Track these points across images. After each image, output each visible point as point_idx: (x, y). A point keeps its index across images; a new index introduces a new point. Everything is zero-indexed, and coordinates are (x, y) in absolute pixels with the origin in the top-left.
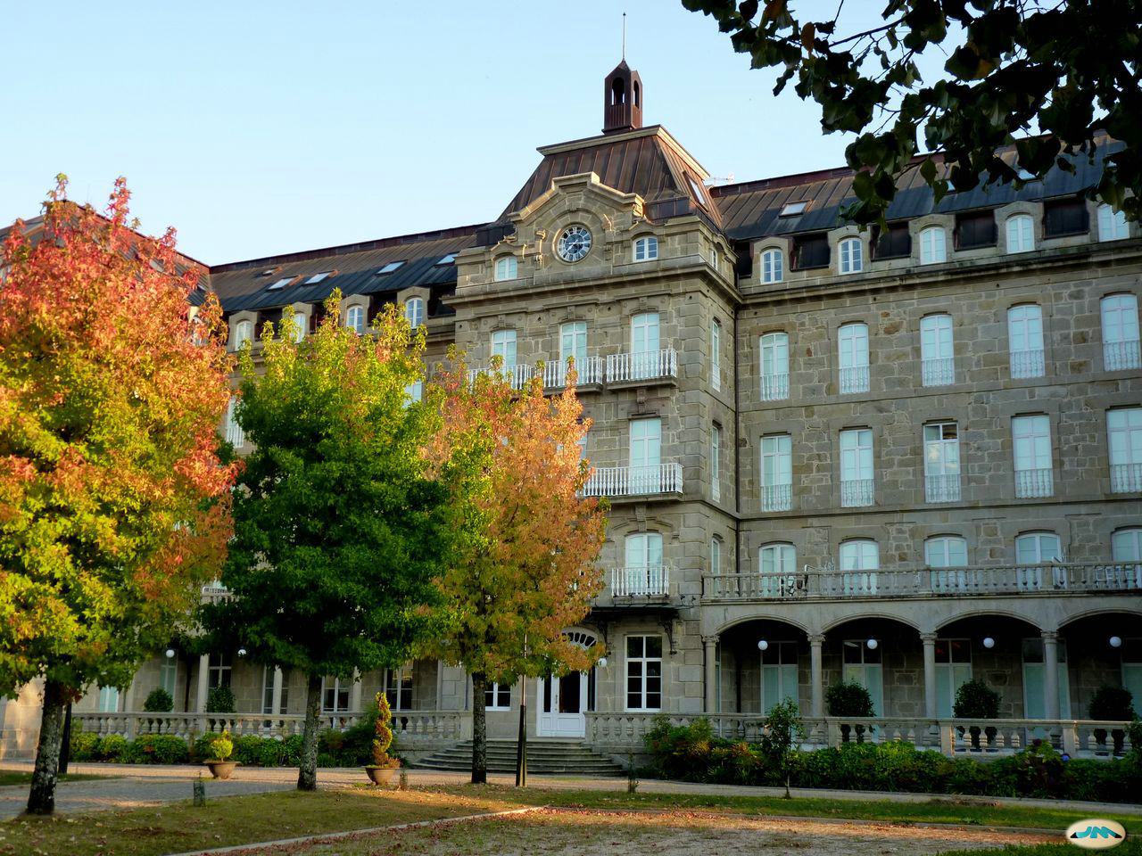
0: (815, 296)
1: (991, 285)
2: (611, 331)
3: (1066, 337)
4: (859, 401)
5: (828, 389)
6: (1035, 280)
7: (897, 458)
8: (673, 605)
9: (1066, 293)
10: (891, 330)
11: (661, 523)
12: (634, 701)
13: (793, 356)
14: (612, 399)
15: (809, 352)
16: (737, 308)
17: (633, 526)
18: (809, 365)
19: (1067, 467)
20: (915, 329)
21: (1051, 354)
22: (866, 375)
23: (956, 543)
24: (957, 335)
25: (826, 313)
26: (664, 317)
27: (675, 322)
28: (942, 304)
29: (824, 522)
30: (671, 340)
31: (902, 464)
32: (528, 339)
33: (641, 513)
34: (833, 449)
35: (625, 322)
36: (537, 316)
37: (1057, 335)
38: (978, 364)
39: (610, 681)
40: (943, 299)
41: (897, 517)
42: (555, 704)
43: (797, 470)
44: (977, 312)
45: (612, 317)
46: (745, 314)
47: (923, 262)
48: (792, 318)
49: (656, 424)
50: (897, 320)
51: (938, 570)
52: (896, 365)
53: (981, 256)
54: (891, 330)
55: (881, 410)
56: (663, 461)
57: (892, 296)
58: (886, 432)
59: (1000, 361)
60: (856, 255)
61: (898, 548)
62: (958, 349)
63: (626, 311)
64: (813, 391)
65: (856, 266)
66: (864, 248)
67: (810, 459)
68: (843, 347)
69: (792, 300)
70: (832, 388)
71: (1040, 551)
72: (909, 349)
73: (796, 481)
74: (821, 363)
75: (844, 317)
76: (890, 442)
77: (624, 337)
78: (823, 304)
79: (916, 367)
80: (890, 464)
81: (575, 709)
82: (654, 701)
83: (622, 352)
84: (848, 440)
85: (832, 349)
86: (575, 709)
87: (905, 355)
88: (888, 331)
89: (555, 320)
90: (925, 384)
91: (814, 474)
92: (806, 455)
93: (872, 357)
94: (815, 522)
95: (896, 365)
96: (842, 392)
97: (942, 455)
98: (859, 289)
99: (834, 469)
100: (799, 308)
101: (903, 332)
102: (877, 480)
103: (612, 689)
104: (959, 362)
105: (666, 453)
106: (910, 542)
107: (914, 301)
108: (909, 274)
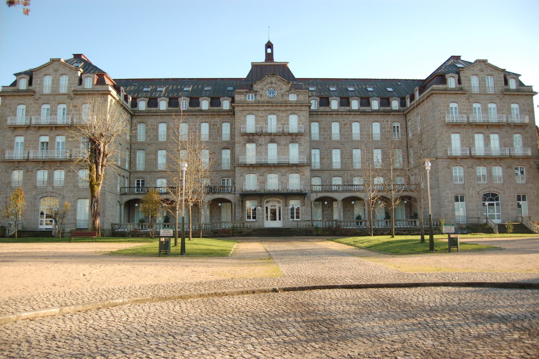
0: (326, 113)
1: (369, 116)
2: (283, 118)
3: (385, 131)
4: (337, 142)
5: (330, 138)
6: (379, 116)
7: (347, 157)
8: (304, 192)
9: (385, 120)
10: (345, 125)
11: (300, 171)
12: (292, 217)
13: (320, 129)
14: (285, 137)
15: (324, 128)
16: (132, 116)
17: (292, 172)
18: (324, 131)
19: (385, 162)
20: (351, 125)
21: (382, 134)
22: (359, 135)
23: (340, 179)
24: (361, 128)
25: (328, 118)
26: (299, 116)
27: (302, 118)
28: (358, 120)
29: (329, 172)
30: (301, 123)
31: (348, 158)
32: (259, 118)
33: (294, 168)
34: (331, 153)
35: (288, 116)
36: (261, 112)
37: (383, 130)
38: (366, 135)
39: (286, 212)
40: (379, 118)
41: (347, 172)
42: (269, 219)
43: (321, 158)
44: (365, 123)
45: (284, 114)
46: (134, 117)
47: (161, 109)
48: (320, 119)
49: (297, 145)
50: (346, 122)
51: (355, 185)
52: (346, 133)
53: (367, 109)
54: (345, 125)
55: (343, 145)
56: (299, 155)
57: (345, 116)
58: (344, 150)
59: (370, 135)
60: (186, 105)
61: (347, 179)
62: (361, 131)
63: (288, 114)
64: (325, 138)
65: (185, 108)
66: (187, 104)
67: (325, 156)
68: (333, 128)
69: (325, 114)
70: (330, 138)
71: (337, 181)
72: (349, 130)
73: (321, 162)
74: (327, 131)
75: (333, 120)
76: (345, 153)
77: (288, 120)
78: (328, 116)
79: (351, 134)
80: (345, 158)
81: (275, 220)
82: (298, 217)
83: (287, 124)
84: (334, 151)
85: (330, 128)
86: (275, 220)
87: (348, 131)
88: (344, 125)
89: (267, 114)
90: (354, 139)
91: (326, 160)
92: (324, 155)
93: (340, 131)
94: (326, 172)
95: (346, 133)
96: (333, 139)
97: (226, 155)
98: (163, 114)
99: (331, 159)
100: (322, 116)
101: (348, 126)
102: (342, 162)
103: (287, 214)
104: (361, 134)
105: (300, 153)
106: (350, 178)
107: (351, 118)
108: (349, 111)
